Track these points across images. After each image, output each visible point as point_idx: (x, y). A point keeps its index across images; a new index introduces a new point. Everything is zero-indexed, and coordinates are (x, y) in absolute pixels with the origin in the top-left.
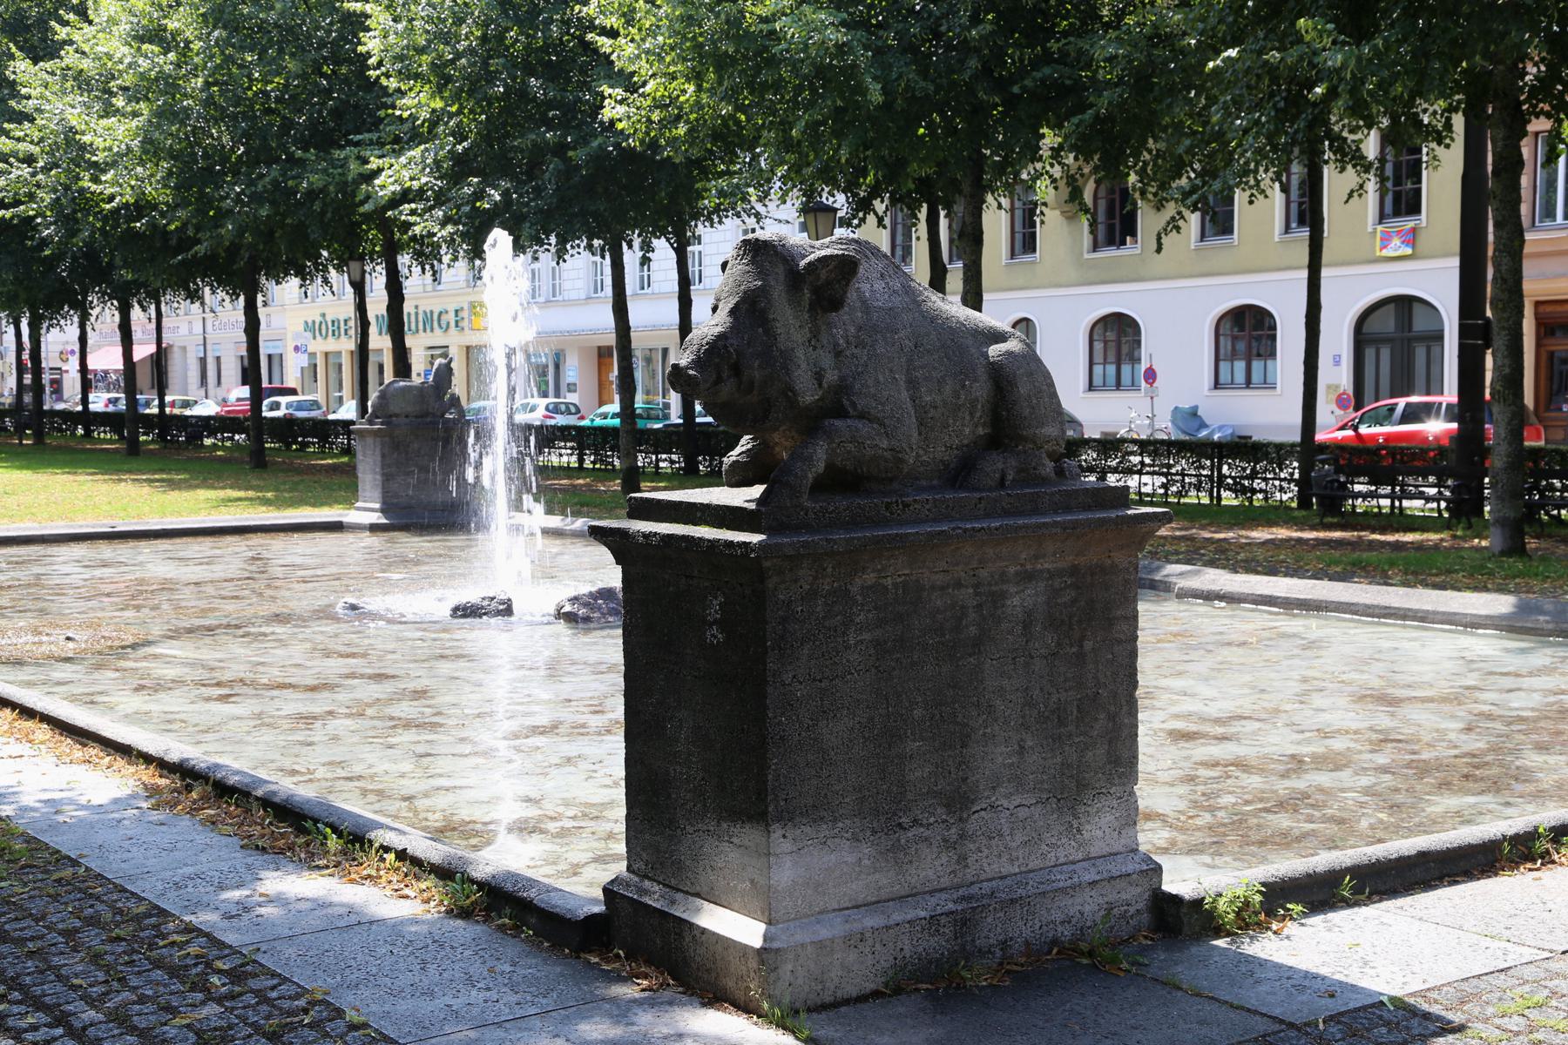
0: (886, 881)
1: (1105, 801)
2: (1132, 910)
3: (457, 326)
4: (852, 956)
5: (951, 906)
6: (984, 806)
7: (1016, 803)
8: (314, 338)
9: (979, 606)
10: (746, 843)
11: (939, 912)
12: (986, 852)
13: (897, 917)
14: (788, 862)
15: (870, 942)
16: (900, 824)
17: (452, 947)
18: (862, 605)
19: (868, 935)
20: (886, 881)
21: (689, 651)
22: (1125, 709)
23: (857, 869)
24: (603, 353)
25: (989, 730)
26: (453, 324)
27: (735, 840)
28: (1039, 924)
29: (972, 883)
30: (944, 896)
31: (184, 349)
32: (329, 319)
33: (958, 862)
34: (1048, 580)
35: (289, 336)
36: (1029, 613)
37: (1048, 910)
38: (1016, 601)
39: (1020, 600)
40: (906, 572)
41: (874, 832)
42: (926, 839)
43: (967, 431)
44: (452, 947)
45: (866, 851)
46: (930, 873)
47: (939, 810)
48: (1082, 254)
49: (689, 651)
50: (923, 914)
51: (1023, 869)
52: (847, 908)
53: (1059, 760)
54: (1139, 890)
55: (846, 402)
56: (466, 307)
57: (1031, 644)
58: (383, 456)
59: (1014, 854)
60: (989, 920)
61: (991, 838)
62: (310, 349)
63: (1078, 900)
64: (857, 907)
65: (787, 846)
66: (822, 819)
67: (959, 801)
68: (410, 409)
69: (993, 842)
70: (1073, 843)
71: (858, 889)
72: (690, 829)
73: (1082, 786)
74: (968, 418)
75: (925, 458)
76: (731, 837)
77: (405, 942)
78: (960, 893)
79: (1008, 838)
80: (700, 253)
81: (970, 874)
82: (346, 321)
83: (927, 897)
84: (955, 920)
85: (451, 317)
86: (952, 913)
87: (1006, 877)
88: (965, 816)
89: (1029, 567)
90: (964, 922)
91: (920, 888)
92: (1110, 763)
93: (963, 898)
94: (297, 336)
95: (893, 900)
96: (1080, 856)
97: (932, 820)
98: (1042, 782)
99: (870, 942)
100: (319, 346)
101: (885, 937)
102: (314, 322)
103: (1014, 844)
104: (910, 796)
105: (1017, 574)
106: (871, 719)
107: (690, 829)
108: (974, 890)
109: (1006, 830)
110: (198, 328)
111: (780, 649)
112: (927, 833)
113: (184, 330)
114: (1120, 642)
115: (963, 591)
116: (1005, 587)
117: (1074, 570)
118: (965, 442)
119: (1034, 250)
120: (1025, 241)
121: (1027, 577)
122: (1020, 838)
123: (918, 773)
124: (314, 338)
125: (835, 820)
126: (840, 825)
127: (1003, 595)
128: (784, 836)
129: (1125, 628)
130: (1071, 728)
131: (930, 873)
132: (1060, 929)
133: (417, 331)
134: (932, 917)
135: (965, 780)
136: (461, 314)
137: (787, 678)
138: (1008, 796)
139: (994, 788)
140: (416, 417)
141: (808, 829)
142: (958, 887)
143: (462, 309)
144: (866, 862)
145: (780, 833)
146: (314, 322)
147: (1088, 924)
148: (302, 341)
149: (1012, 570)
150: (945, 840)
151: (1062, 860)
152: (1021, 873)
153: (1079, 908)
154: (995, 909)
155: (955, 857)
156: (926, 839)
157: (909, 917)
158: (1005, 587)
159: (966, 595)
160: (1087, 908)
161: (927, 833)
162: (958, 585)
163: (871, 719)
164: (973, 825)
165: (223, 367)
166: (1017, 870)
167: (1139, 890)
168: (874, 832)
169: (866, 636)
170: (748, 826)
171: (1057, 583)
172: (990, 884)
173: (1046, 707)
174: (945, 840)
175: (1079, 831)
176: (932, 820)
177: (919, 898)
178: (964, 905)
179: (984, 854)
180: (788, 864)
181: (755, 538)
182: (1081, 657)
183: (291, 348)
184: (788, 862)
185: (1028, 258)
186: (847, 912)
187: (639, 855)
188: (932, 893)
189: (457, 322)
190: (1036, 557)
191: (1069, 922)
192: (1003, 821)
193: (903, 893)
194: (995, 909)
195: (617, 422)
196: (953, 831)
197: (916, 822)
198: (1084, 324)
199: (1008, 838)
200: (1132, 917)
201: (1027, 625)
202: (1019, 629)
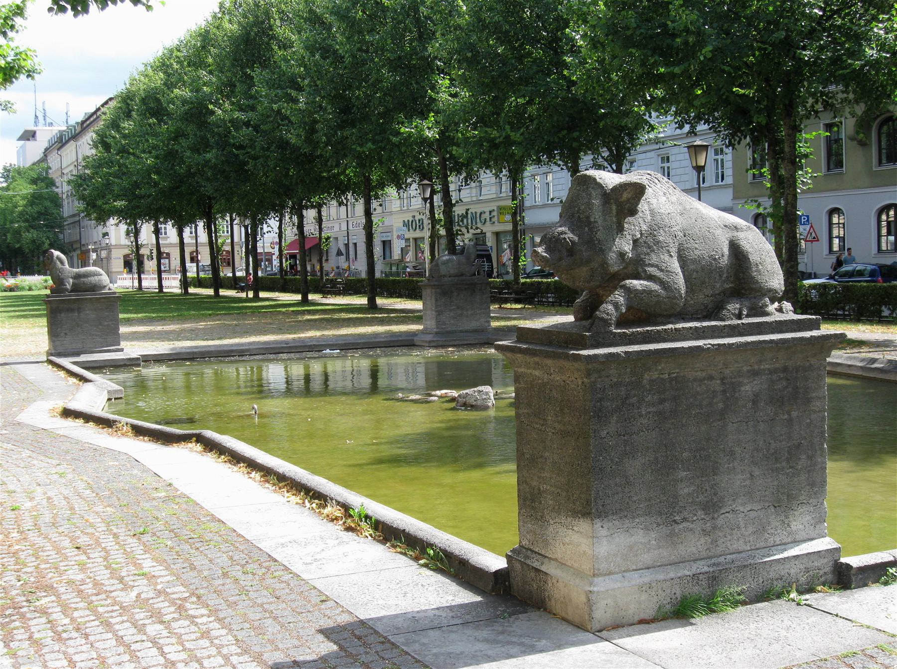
0: (666, 554)
1: (804, 508)
2: (821, 572)
3: (490, 220)
4: (644, 597)
5: (706, 569)
6: (728, 510)
7: (749, 509)
8: (409, 230)
9: (724, 391)
10: (581, 530)
11: (699, 572)
12: (729, 537)
13: (672, 575)
14: (605, 542)
15: (655, 588)
16: (674, 520)
17: (422, 585)
18: (650, 391)
19: (654, 585)
20: (666, 554)
21: (550, 418)
22: (819, 452)
23: (648, 546)
24: (143, 272)
25: (731, 465)
26: (488, 219)
27: (575, 528)
28: (762, 580)
29: (721, 556)
30: (702, 563)
31: (336, 239)
32: (417, 219)
33: (712, 543)
34: (768, 374)
35: (395, 229)
36: (756, 395)
37: (768, 572)
38: (748, 388)
39: (748, 388)
40: (677, 371)
41: (658, 525)
42: (691, 530)
43: (718, 285)
44: (422, 585)
45: (654, 536)
46: (694, 549)
47: (699, 513)
48: (872, 168)
49: (550, 418)
50: (688, 573)
51: (753, 548)
52: (642, 569)
53: (776, 483)
54: (826, 560)
55: (640, 270)
56: (496, 209)
57: (757, 414)
58: (436, 300)
59: (747, 539)
60: (730, 577)
61: (732, 529)
62: (406, 237)
63: (787, 566)
64: (648, 568)
65: (604, 532)
66: (626, 517)
67: (712, 507)
68: (452, 272)
69: (734, 532)
70: (785, 533)
71: (647, 558)
72: (552, 522)
73: (790, 497)
74: (718, 278)
75: (692, 302)
76: (573, 526)
77: (397, 581)
78: (713, 561)
79: (743, 529)
80: (668, 168)
81: (719, 550)
82: (490, 212)
83: (692, 563)
84: (709, 577)
85: (487, 216)
86: (706, 573)
87: (741, 552)
88: (716, 516)
89: (756, 367)
90: (714, 578)
91: (687, 558)
92: (809, 485)
93: (714, 564)
94: (399, 229)
95: (670, 565)
96: (789, 540)
97: (695, 518)
98: (765, 496)
99: (655, 588)
100: (411, 235)
101: (664, 586)
102: (408, 221)
103: (747, 533)
104: (681, 504)
105: (749, 371)
106: (656, 458)
107: (552, 522)
108: (722, 559)
109: (742, 525)
110: (344, 227)
111: (599, 416)
112: (692, 526)
113: (336, 228)
114: (815, 412)
115: (714, 381)
116: (741, 379)
117: (785, 369)
118: (717, 292)
119: (842, 167)
120: (834, 159)
121: (755, 373)
122: (751, 529)
123: (684, 490)
124: (409, 230)
125: (634, 517)
126: (637, 520)
127: (740, 384)
128: (602, 527)
129: (818, 404)
130: (784, 464)
131: (694, 549)
132: (775, 583)
133: (416, 229)
134: (694, 575)
135: (715, 494)
136: (493, 214)
137: (604, 433)
138: (743, 504)
139: (734, 500)
140: (456, 276)
141: (616, 522)
142: (710, 558)
143: (494, 210)
144: (654, 542)
145: (599, 525)
146: (408, 221)
147: (793, 580)
148: (402, 233)
149: (745, 369)
150: (703, 530)
151: (778, 542)
152: (751, 550)
153: (788, 571)
154: (734, 571)
155: (710, 540)
156: (691, 530)
157: (679, 575)
158: (741, 379)
159: (716, 385)
160: (792, 571)
161: (692, 526)
162: (711, 378)
163: (656, 458)
164: (720, 522)
165: (358, 249)
166: (749, 548)
167: (826, 560)
168: (658, 525)
169: (652, 409)
170: (581, 520)
171: (775, 377)
172: (731, 556)
173: (768, 451)
174: (703, 530)
175: (789, 525)
176: (695, 518)
177: (687, 564)
178: (715, 568)
179: (728, 539)
180: (605, 543)
181: (572, 352)
182: (790, 421)
183: (395, 237)
184: (605, 542)
185: (837, 171)
186: (641, 571)
187: (525, 536)
188: (695, 560)
189: (490, 218)
190: (761, 361)
191: (781, 579)
192: (740, 519)
193: (677, 561)
194: (734, 571)
195: (121, 316)
196: (708, 524)
197: (685, 519)
198: (876, 209)
199: (743, 529)
200: (821, 576)
201: (755, 402)
202: (750, 405)
